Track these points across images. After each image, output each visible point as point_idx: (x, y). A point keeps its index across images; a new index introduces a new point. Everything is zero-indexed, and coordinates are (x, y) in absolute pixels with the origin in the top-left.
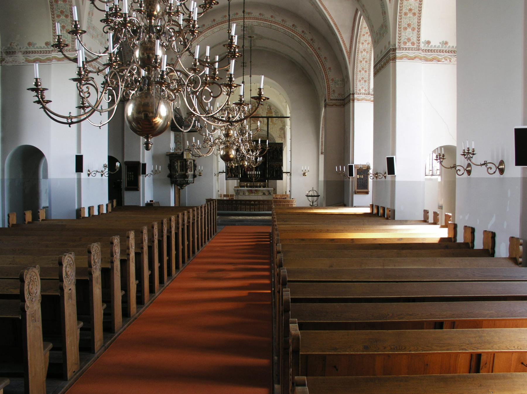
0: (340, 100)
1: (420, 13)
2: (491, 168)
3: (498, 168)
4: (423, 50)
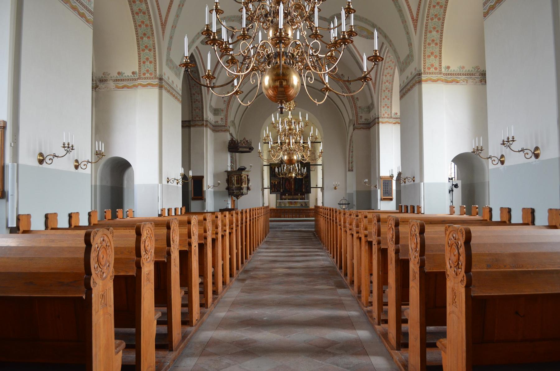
0: (366, 124)
1: (441, 43)
2: (528, 154)
3: (534, 153)
4: (444, 74)
